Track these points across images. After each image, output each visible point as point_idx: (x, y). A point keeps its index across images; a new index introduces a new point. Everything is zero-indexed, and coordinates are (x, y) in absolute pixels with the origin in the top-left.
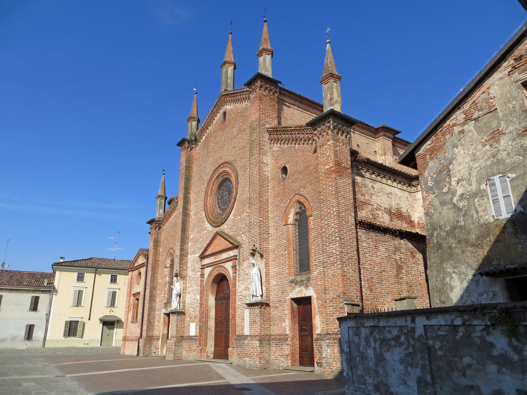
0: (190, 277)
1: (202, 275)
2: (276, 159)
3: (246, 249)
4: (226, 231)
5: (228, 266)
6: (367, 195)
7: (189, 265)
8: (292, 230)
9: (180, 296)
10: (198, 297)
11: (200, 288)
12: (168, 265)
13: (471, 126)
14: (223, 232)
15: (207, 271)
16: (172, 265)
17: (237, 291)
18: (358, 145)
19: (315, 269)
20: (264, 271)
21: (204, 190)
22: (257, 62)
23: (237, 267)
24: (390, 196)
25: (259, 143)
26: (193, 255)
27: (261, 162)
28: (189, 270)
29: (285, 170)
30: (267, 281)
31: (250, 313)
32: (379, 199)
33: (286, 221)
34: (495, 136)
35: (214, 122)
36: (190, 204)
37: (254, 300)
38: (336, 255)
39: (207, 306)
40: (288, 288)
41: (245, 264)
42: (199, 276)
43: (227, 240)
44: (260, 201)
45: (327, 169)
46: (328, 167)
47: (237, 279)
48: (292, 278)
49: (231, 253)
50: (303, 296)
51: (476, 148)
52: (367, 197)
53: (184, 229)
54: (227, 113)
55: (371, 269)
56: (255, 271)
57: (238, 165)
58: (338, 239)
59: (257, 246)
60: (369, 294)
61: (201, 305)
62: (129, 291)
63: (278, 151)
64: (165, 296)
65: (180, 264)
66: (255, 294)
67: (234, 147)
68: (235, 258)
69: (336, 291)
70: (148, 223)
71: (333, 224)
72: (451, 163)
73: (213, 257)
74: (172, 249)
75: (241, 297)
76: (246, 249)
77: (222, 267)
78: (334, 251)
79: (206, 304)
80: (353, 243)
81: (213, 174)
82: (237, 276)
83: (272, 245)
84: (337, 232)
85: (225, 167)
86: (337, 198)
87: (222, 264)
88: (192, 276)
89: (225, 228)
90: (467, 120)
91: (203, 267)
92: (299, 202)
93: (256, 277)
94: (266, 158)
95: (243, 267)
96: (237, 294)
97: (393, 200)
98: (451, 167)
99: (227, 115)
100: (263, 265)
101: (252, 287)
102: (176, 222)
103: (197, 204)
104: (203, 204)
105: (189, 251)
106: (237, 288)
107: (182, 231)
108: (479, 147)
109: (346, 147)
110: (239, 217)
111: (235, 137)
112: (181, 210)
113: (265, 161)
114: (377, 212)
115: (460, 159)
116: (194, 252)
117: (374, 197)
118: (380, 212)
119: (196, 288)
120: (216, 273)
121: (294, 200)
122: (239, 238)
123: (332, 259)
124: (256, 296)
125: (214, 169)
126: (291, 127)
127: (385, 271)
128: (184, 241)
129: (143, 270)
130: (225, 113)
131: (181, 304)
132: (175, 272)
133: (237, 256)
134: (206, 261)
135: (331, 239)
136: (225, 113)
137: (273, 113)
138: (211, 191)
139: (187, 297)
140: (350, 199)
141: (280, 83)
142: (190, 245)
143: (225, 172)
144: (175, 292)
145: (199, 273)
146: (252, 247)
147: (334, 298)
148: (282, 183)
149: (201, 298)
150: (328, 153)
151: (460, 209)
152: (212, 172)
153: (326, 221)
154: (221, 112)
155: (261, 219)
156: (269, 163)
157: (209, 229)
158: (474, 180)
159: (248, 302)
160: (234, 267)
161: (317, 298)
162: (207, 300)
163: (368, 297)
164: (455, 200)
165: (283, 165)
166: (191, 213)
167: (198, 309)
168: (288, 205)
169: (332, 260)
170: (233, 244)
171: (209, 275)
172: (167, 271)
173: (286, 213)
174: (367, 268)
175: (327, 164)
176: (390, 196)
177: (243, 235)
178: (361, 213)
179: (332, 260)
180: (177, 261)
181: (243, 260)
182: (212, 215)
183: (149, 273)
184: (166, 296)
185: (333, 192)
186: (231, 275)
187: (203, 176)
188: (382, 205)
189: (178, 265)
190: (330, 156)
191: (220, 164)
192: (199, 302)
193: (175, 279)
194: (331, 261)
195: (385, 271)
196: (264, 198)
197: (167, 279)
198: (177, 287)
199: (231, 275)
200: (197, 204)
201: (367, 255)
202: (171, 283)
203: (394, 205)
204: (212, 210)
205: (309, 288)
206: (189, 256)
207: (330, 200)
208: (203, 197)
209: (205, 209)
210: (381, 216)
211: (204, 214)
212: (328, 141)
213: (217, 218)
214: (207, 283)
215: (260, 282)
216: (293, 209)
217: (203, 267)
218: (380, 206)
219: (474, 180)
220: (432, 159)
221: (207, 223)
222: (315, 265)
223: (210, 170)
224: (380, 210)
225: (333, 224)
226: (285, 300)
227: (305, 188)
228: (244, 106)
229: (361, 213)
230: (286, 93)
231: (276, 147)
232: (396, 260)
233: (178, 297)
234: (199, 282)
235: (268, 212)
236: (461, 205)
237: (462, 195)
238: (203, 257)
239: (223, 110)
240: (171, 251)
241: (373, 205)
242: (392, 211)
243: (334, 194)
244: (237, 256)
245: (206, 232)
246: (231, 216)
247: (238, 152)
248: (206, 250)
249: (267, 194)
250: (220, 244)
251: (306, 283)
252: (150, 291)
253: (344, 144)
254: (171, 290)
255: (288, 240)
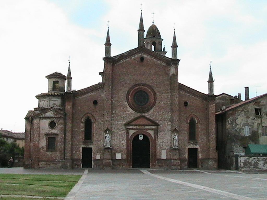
13: (243, 112)
22: (143, 139)
34: (248, 117)
51: (243, 118)
62: (36, 181)
72: (236, 119)
90: (242, 111)
98: (236, 120)
108: (244, 118)
115: (239, 119)
151: (237, 131)
157: (131, 113)
158: (241, 126)
164: (236, 128)
219: (241, 126)
220: (231, 116)
221: (129, 108)
236: (237, 130)
237: (238, 128)
248: (129, 123)
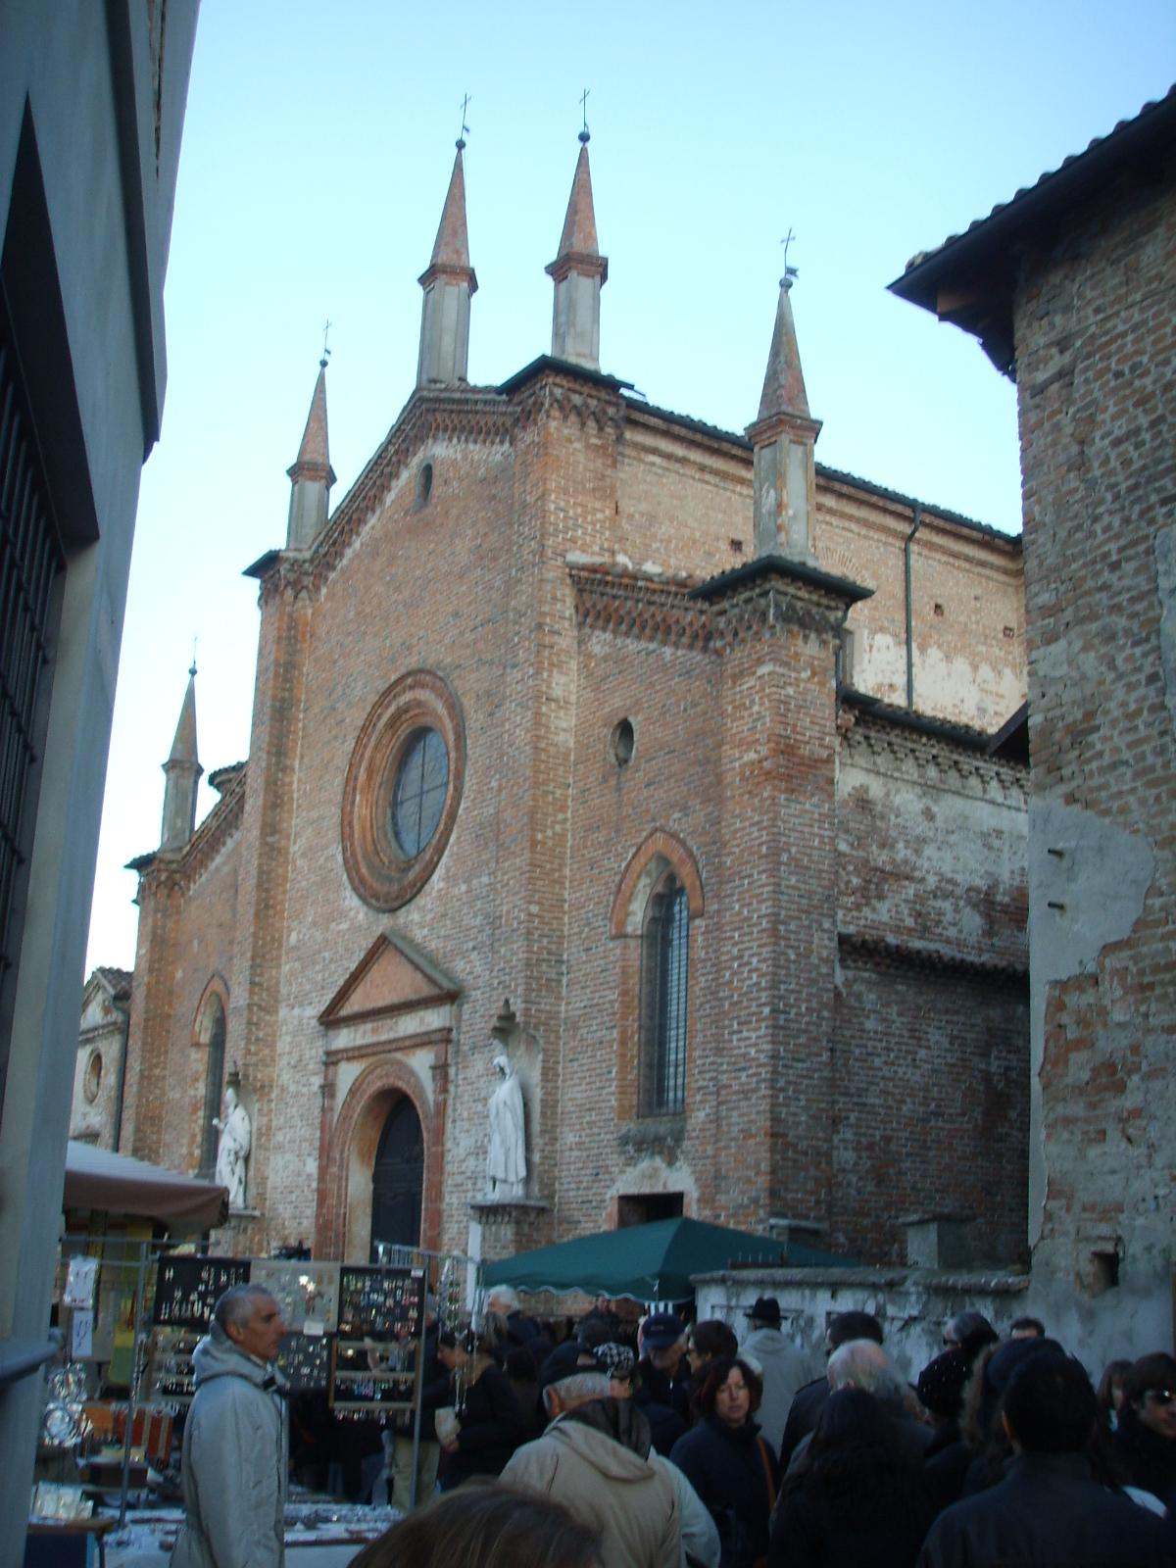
0: (283, 1089)
1: (328, 1089)
2: (596, 682)
3: (477, 1016)
4: (418, 934)
5: (421, 1062)
6: (901, 845)
7: (283, 1044)
8: (635, 953)
9: (247, 1159)
10: (312, 1166)
11: (318, 1134)
12: (205, 1038)
14: (404, 938)
15: (348, 1074)
16: (218, 1043)
17: (449, 1157)
18: (938, 607)
19: (701, 1102)
20: (537, 1094)
21: (341, 761)
23: (452, 1071)
24: (996, 843)
25: (540, 626)
26: (296, 1011)
27: (540, 697)
28: (283, 1062)
29: (625, 730)
30: (551, 1133)
31: (484, 1239)
32: (948, 856)
33: (622, 924)
35: (390, 498)
36: (290, 812)
37: (494, 1196)
38: (758, 1066)
39: (342, 1197)
40: (614, 1160)
41: (478, 1064)
42: (315, 1088)
43: (417, 967)
44: (534, 843)
45: (752, 763)
46: (752, 756)
47: (449, 1111)
48: (630, 1126)
49: (434, 1019)
50: (659, 1189)
52: (902, 852)
53: (267, 908)
54: (436, 472)
55: (890, 1107)
56: (505, 1092)
57: (469, 685)
58: (766, 1010)
59: (517, 1006)
60: (871, 1193)
61: (322, 1196)
63: (605, 659)
64: (191, 1154)
65: (248, 1041)
66: (500, 1175)
67: (456, 615)
68: (443, 1038)
69: (748, 1181)
70: (127, 866)
71: (755, 960)
73: (369, 1026)
74: (222, 978)
75: (459, 1179)
76: (477, 1016)
77: (400, 1063)
78: (753, 1052)
79: (339, 1197)
80: (819, 1026)
81: (377, 705)
82: (450, 1102)
83: (572, 1003)
84: (765, 989)
85: (423, 686)
86: (773, 872)
87: (398, 1055)
88: (292, 1088)
89: (417, 920)
91: (332, 1059)
92: (663, 860)
93: (509, 1115)
94: (563, 679)
95: (471, 1074)
96: (449, 1168)
97: (1006, 855)
99: (436, 481)
100: (535, 1076)
101: (495, 1151)
102: (235, 872)
103: (314, 814)
104: (336, 819)
105: (284, 991)
106: (449, 1145)
107: (257, 914)
109: (822, 684)
110: (464, 888)
111: (461, 576)
112: (256, 833)
113: (557, 692)
114: (938, 903)
116: (302, 1001)
117: (929, 851)
118: (946, 905)
119: (306, 1132)
120: (376, 1085)
121: (650, 849)
122: (459, 967)
123: (744, 1075)
124: (505, 1181)
125: (382, 686)
126: (652, 581)
127: (941, 1115)
128: (264, 955)
129: (110, 1049)
130: (428, 472)
131: (253, 1191)
132: (228, 1068)
133: (450, 1030)
134: (344, 1038)
135: (746, 1008)
136: (428, 472)
137: (598, 505)
138: (371, 773)
139: (272, 1163)
140: (821, 871)
141: (631, 387)
142: (286, 968)
143: (419, 704)
144: (226, 1144)
145: (317, 1081)
146: (497, 1008)
147: (741, 1206)
148: (613, 782)
149: (323, 1171)
150: (756, 708)
152: (373, 698)
153: (735, 944)
154: (416, 462)
155: (534, 909)
156: (573, 699)
157: (356, 920)
159: (479, 1199)
160: (441, 1070)
161: (699, 1201)
162: (342, 1179)
163: (867, 1201)
165: (621, 716)
166: (293, 849)
167: (310, 1211)
168: (628, 866)
169: (744, 1079)
170: (440, 987)
171: (352, 1092)
172: (198, 1060)
173: (622, 894)
174: (873, 1106)
175: (750, 745)
176: (996, 843)
177: (474, 956)
178: (874, 910)
179: (744, 1079)
180: (235, 1027)
181: (474, 1048)
182: (371, 867)
183: (135, 1065)
184: (197, 1152)
185: (764, 849)
186: (430, 1096)
187: (340, 706)
188: (959, 878)
189: (242, 1044)
190: (760, 717)
191: (403, 670)
192: (314, 1185)
193: (229, 1094)
194: (742, 1085)
195: (941, 1115)
196: (549, 833)
197: (201, 1089)
198: (236, 1126)
199: (430, 1096)
200: (314, 814)
201: (878, 1062)
202: (215, 1107)
203: (1006, 876)
204: (370, 848)
205: (678, 1164)
206: (283, 1012)
207: (751, 875)
208: (339, 790)
209: (346, 837)
210: (949, 916)
211: (340, 858)
212: (760, 662)
213: (391, 880)
214: (345, 1117)
215: (521, 1135)
216: (644, 881)
217: (332, 1059)
218: (952, 881)
221: (348, 893)
222: (700, 1088)
223: (364, 689)
224: (946, 896)
225: (755, 960)
226: (603, 1201)
227: (685, 810)
228: (499, 457)
229: (874, 910)
230: (654, 421)
231: (600, 642)
232: (987, 1077)
233: (240, 1163)
234: (317, 1112)
235: (560, 882)
238: (331, 1019)
239: (420, 455)
240: (217, 985)
241: (922, 880)
242: (999, 898)
243: (766, 856)
244: (450, 1030)
245: (344, 926)
246: (435, 877)
247: (469, 637)
249: (560, 817)
250: (391, 982)
251: (666, 1147)
252: (137, 1130)
253: (814, 674)
254: (212, 1137)
255: (624, 993)
